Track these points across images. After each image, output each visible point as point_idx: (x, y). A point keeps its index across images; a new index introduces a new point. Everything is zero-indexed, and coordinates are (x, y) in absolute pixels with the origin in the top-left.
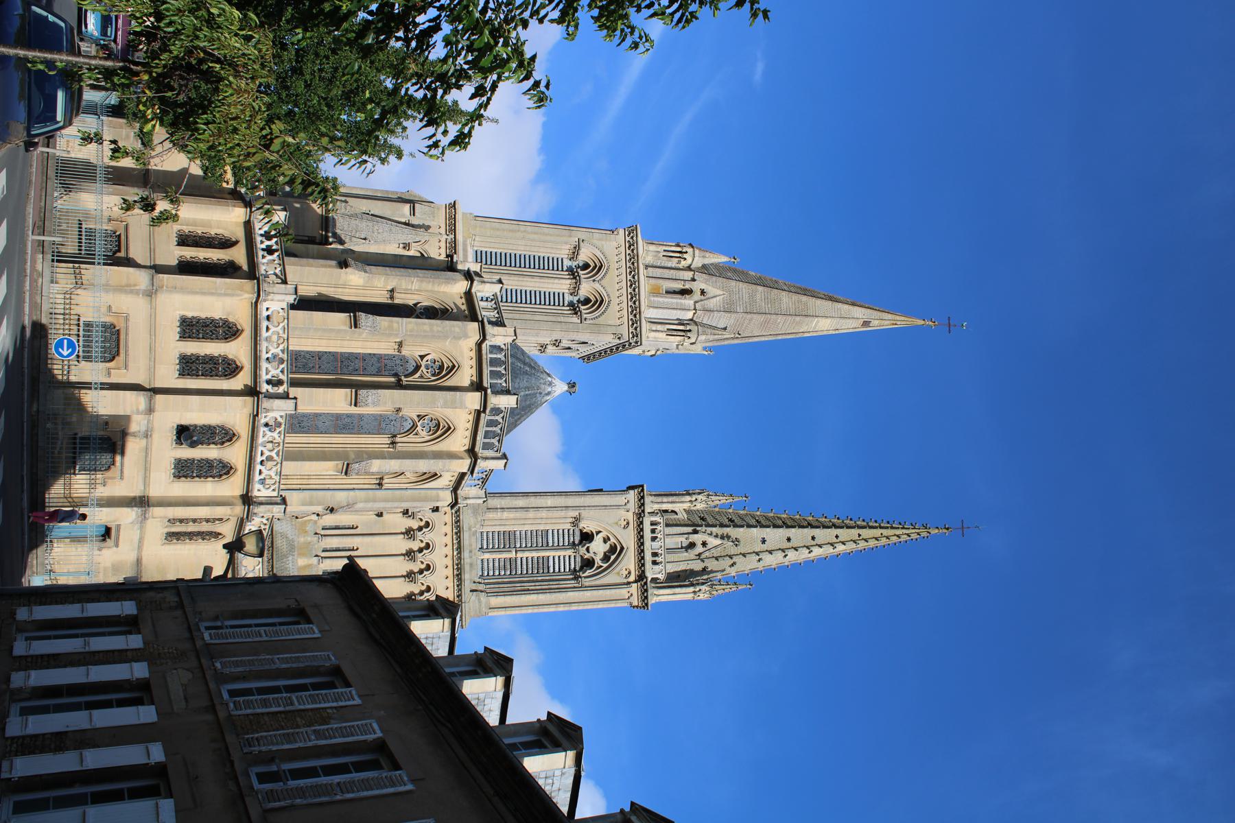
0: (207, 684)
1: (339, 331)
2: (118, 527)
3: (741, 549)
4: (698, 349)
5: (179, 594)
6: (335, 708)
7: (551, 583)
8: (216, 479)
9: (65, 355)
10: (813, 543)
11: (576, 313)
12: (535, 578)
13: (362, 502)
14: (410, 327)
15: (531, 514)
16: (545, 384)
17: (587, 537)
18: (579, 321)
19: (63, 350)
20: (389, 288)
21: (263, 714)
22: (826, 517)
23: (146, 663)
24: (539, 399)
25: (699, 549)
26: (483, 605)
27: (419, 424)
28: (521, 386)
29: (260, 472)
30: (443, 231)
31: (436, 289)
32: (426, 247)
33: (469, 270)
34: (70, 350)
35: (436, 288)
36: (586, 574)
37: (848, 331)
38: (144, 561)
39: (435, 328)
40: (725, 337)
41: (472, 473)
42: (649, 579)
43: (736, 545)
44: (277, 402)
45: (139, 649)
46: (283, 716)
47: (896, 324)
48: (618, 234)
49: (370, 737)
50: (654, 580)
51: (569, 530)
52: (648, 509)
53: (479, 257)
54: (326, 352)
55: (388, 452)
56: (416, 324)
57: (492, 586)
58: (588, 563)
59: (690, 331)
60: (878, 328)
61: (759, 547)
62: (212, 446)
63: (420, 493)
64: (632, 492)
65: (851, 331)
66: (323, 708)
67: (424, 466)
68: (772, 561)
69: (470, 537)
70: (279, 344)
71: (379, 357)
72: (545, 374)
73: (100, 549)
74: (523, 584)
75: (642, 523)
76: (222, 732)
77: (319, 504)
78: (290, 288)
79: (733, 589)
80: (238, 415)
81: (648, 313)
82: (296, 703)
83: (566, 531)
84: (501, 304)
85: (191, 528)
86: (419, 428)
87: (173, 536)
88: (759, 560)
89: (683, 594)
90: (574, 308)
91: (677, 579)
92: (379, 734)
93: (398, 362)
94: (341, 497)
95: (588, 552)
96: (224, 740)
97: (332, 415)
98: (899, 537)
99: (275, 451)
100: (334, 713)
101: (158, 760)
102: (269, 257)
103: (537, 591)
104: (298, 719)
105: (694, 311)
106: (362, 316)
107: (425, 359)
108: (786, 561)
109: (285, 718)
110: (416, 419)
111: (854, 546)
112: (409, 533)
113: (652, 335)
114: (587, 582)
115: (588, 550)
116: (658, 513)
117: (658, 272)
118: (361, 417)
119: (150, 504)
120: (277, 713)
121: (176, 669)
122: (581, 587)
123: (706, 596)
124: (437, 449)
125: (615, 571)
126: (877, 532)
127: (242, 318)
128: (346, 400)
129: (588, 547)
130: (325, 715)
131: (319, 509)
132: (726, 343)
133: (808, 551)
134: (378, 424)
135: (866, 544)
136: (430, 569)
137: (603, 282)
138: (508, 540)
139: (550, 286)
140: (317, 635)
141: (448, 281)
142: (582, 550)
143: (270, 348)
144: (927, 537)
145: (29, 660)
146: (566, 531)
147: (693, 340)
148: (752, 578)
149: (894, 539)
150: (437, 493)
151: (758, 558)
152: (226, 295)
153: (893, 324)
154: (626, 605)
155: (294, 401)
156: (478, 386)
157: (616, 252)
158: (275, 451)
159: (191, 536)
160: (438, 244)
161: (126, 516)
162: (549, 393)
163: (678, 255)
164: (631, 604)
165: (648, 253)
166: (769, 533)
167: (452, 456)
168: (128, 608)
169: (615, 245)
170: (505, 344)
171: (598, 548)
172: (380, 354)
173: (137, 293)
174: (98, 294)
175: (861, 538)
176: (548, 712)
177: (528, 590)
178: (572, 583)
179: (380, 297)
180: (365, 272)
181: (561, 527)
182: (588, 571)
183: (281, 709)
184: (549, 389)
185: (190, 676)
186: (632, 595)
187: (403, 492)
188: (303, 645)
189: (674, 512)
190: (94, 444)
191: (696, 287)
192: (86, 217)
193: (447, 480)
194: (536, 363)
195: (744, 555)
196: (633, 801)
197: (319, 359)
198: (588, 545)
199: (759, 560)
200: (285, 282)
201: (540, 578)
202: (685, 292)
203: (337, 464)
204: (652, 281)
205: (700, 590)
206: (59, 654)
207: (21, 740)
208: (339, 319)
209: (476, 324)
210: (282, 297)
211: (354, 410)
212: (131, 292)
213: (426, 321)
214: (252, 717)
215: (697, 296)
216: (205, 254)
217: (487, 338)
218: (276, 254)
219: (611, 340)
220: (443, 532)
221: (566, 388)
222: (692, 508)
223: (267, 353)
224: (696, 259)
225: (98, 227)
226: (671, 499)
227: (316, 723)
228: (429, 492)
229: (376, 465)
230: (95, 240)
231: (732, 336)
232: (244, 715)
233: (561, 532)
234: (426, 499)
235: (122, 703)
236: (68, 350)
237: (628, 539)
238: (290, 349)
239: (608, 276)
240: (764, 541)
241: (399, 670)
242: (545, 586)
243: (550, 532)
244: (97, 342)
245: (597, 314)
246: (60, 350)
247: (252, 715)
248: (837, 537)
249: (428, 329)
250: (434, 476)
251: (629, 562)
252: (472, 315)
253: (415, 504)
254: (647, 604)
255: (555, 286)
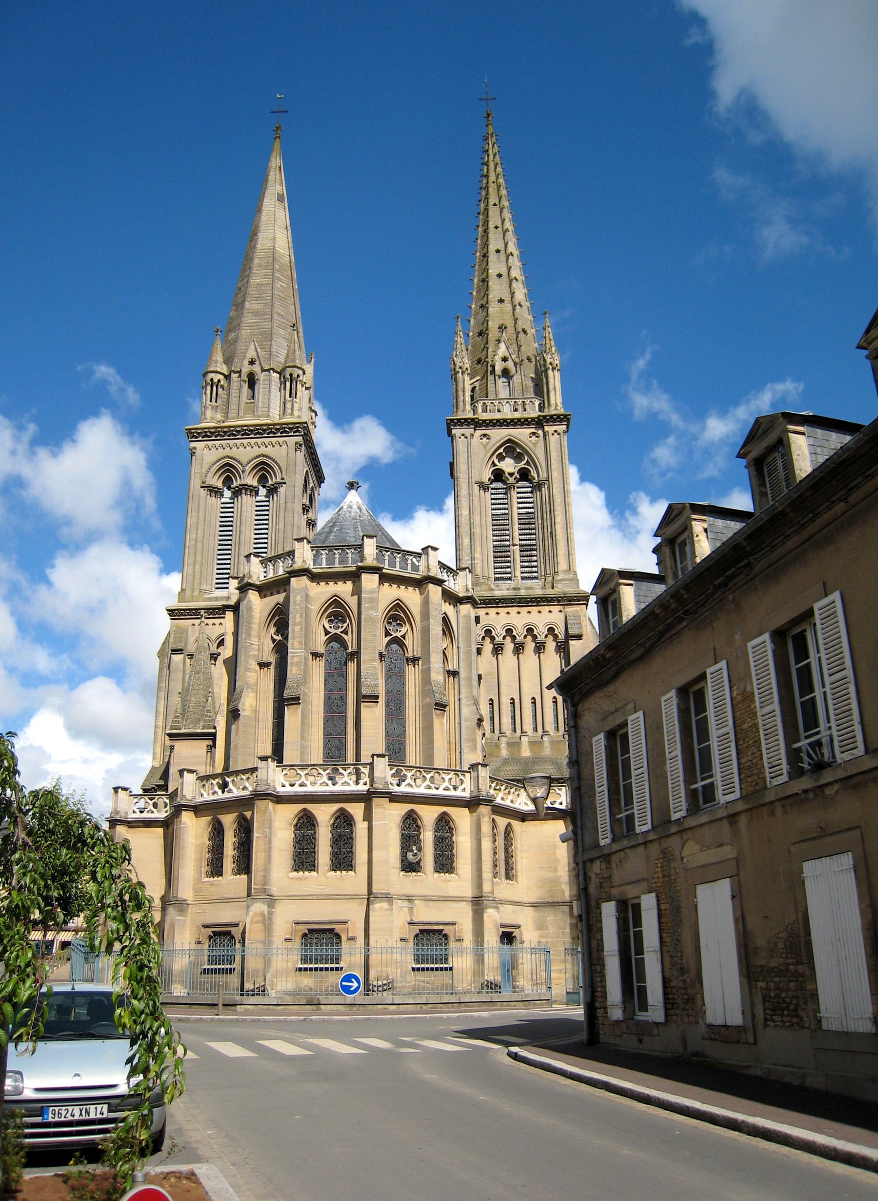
0: (701, 825)
1: (304, 716)
2: (502, 926)
3: (509, 323)
4: (309, 369)
5: (592, 860)
6: (731, 687)
7: (544, 510)
8: (454, 832)
9: (357, 985)
10: (503, 252)
11: (276, 488)
12: (540, 526)
13: (472, 692)
14: (296, 645)
15: (477, 530)
16: (350, 512)
17: (498, 476)
18: (284, 485)
19: (352, 987)
20: (258, 667)
21: (739, 764)
22: (477, 239)
23: (809, 868)
24: (365, 517)
25: (510, 364)
26: (567, 577)
27: (394, 635)
28: (353, 535)
29: (446, 789)
30: (197, 622)
31: (258, 621)
32: (213, 638)
33: (238, 589)
34: (353, 980)
35: (257, 620)
36: (535, 476)
37: (288, 216)
38: (534, 900)
39: (298, 620)
40: (296, 339)
41: (442, 581)
42: (540, 414)
43: (506, 328)
44: (377, 773)
45: (657, 896)
46: (741, 743)
47: (280, 168)
48: (195, 448)
49: (769, 647)
50: (541, 408)
51: (492, 494)
52: (470, 415)
53: (222, 585)
54: (324, 728)
55: (422, 666)
56: (293, 639)
57: (548, 568)
58: (524, 475)
59: (291, 375)
60: (284, 185)
61: (508, 307)
62: (421, 837)
63: (462, 634)
64: (454, 431)
65: (287, 213)
66: (732, 701)
67: (436, 628)
68: (520, 293)
69: (501, 590)
70: (319, 773)
71: (328, 676)
72: (340, 512)
73: (522, 942)
74: (546, 538)
75: (484, 421)
76: (763, 805)
77: (474, 733)
78: (260, 764)
79: (550, 331)
80: (391, 812)
81: (275, 416)
82: (721, 732)
83: (493, 496)
84: (269, 556)
85: (501, 855)
86: (399, 635)
87: (509, 874)
88: (520, 305)
89: (555, 380)
90: (272, 491)
91: (540, 388)
92: (766, 637)
93: (333, 657)
94: (467, 711)
95: (513, 474)
96: (772, 802)
97: (387, 720)
98: (497, 164)
99: (425, 775)
100: (738, 688)
101: (824, 864)
102: (231, 786)
103: (553, 525)
104: (745, 726)
105: (272, 371)
106: (287, 693)
107: (329, 630)
108: (521, 278)
109: (744, 740)
110: (389, 638)
111: (505, 211)
112: (498, 650)
113: (296, 413)
114: (543, 475)
115: (511, 475)
116: (475, 406)
117: (233, 406)
118: (388, 692)
119: (480, 895)
120: (737, 749)
121: (682, 858)
122: (548, 481)
123: (556, 358)
124: (419, 616)
125: (533, 448)
126: (492, 188)
127: (291, 811)
128: (372, 707)
129: (509, 474)
130: (739, 698)
131: (479, 733)
132: (302, 339)
133: (510, 257)
134: (395, 676)
135: (503, 198)
136: (533, 629)
137: (244, 462)
138: (501, 554)
139: (249, 509)
140: (640, 714)
141: (250, 609)
142: (511, 480)
143: (318, 784)
144: (497, 135)
145: (669, 1006)
146: (493, 496)
147: (301, 372)
148: (539, 314)
149: (499, 169)
150: (462, 617)
151: (518, 307)
152: (270, 827)
153: (280, 170)
154: (565, 437)
155: (375, 757)
156: (354, 576)
157: (214, 450)
158: (425, 775)
159: (509, 856)
160: (210, 626)
161: (492, 917)
162: (360, 508)
163: (215, 388)
164: (564, 432)
165: (211, 419)
166: (493, 295)
167: (426, 603)
168: (609, 911)
169: (206, 450)
170: (312, 550)
171: (509, 466)
172: (325, 675)
173: (270, 914)
174: (275, 951)
175: (497, 203)
176: (737, 457)
177: (551, 533)
178: (545, 490)
179: (268, 678)
180: (242, 691)
181: (489, 502)
182: (532, 474)
183: (733, 745)
184: (355, 507)
185: (690, 843)
186: (555, 431)
187: (461, 650)
188: (654, 729)
189: (473, 390)
190: (441, 950)
191: (246, 369)
192: (198, 964)
193: (449, 609)
194: (329, 521)
195: (516, 320)
196: (856, 346)
197: (331, 734)
198: (507, 475)
199: (520, 305)
200: (254, 770)
201: (540, 522)
202: (252, 381)
203: (436, 715)
204: (242, 413)
205: (551, 364)
206: (664, 978)
207: (767, 1011)
208: (291, 716)
209: (293, 580)
210: (270, 770)
211: (382, 700)
212: (270, 919)
213: (290, 628)
214: (743, 775)
215: (256, 368)
216: (230, 849)
217: (306, 567)
218: (227, 779)
219: (303, 453)
220: (496, 616)
221: (353, 492)
222: (469, 371)
223: (327, 785)
224: (219, 370)
225: (206, 953)
226: (460, 393)
227: (750, 706)
228: (461, 625)
229: (437, 676)
230: (223, 956)
231: (296, 333)
232: (740, 784)
233: (493, 501)
234: (468, 629)
235: (638, 922)
236: (352, 982)
237: (499, 435)
238: (321, 763)
239: (237, 457)
240: (501, 301)
241: (684, 624)
242: (547, 516)
243: (494, 512)
244: (327, 951)
245: (276, 468)
246: (352, 989)
247: (740, 775)
248: (496, 227)
249: (299, 626)
250: (446, 620)
251: (522, 434)
252: (280, 585)
253: (473, 639)
254: (565, 416)
255: (249, 509)
